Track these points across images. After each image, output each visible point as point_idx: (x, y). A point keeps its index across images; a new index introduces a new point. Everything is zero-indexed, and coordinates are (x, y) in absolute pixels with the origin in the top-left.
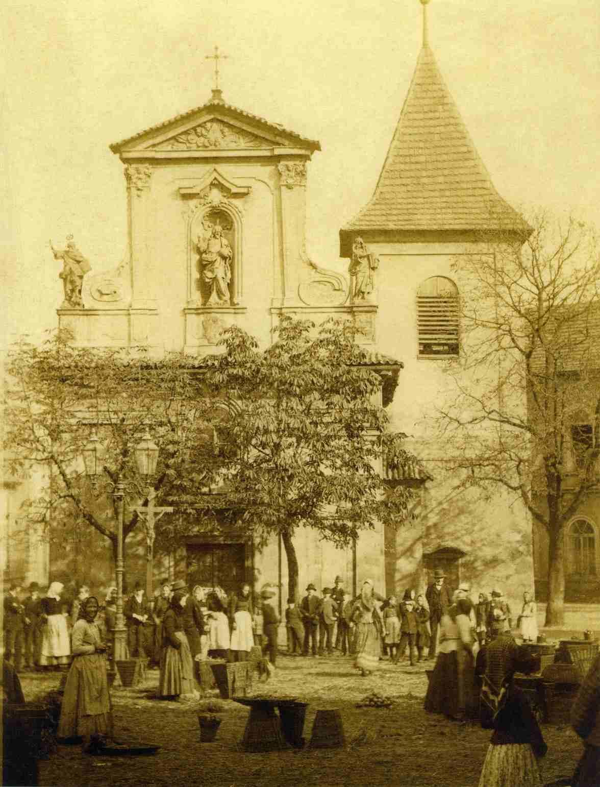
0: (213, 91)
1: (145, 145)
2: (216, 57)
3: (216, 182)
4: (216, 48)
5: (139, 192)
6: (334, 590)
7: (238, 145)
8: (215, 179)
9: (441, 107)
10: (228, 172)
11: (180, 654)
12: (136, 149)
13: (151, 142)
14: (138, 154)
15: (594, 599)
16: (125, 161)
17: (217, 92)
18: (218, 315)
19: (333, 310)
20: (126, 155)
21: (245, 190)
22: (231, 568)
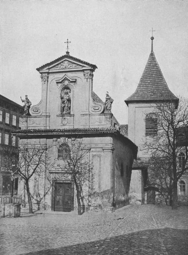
0: (66, 52)
1: (47, 68)
2: (68, 42)
3: (66, 78)
4: (68, 40)
5: (45, 82)
6: (93, 188)
7: (73, 67)
8: (66, 77)
9: (155, 170)
10: (70, 75)
11: (28, 213)
12: (43, 70)
13: (48, 67)
14: (46, 70)
15: (177, 99)
16: (41, 73)
17: (68, 53)
18: (66, 117)
19: (99, 115)
20: (41, 72)
21: (75, 80)
22: (157, 199)
